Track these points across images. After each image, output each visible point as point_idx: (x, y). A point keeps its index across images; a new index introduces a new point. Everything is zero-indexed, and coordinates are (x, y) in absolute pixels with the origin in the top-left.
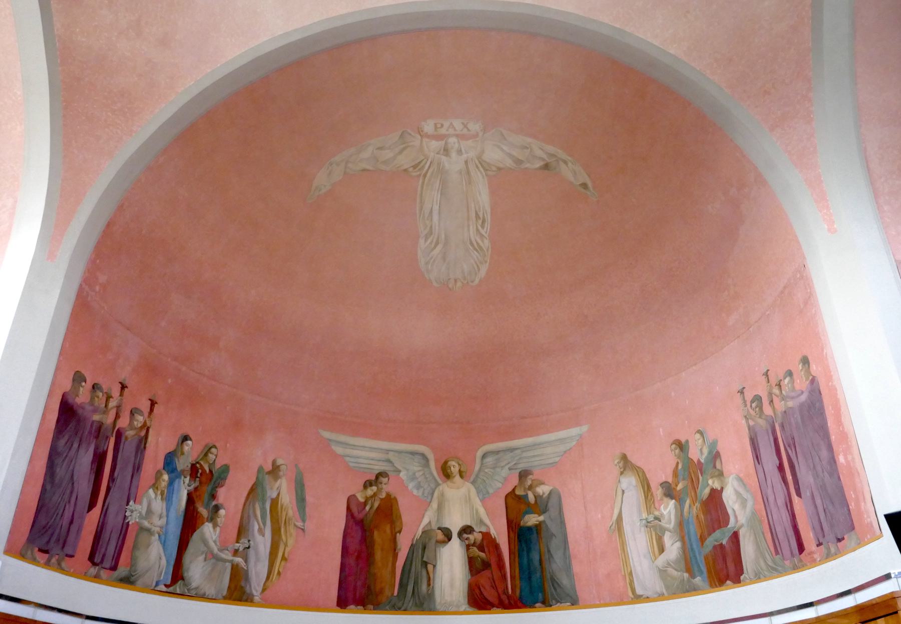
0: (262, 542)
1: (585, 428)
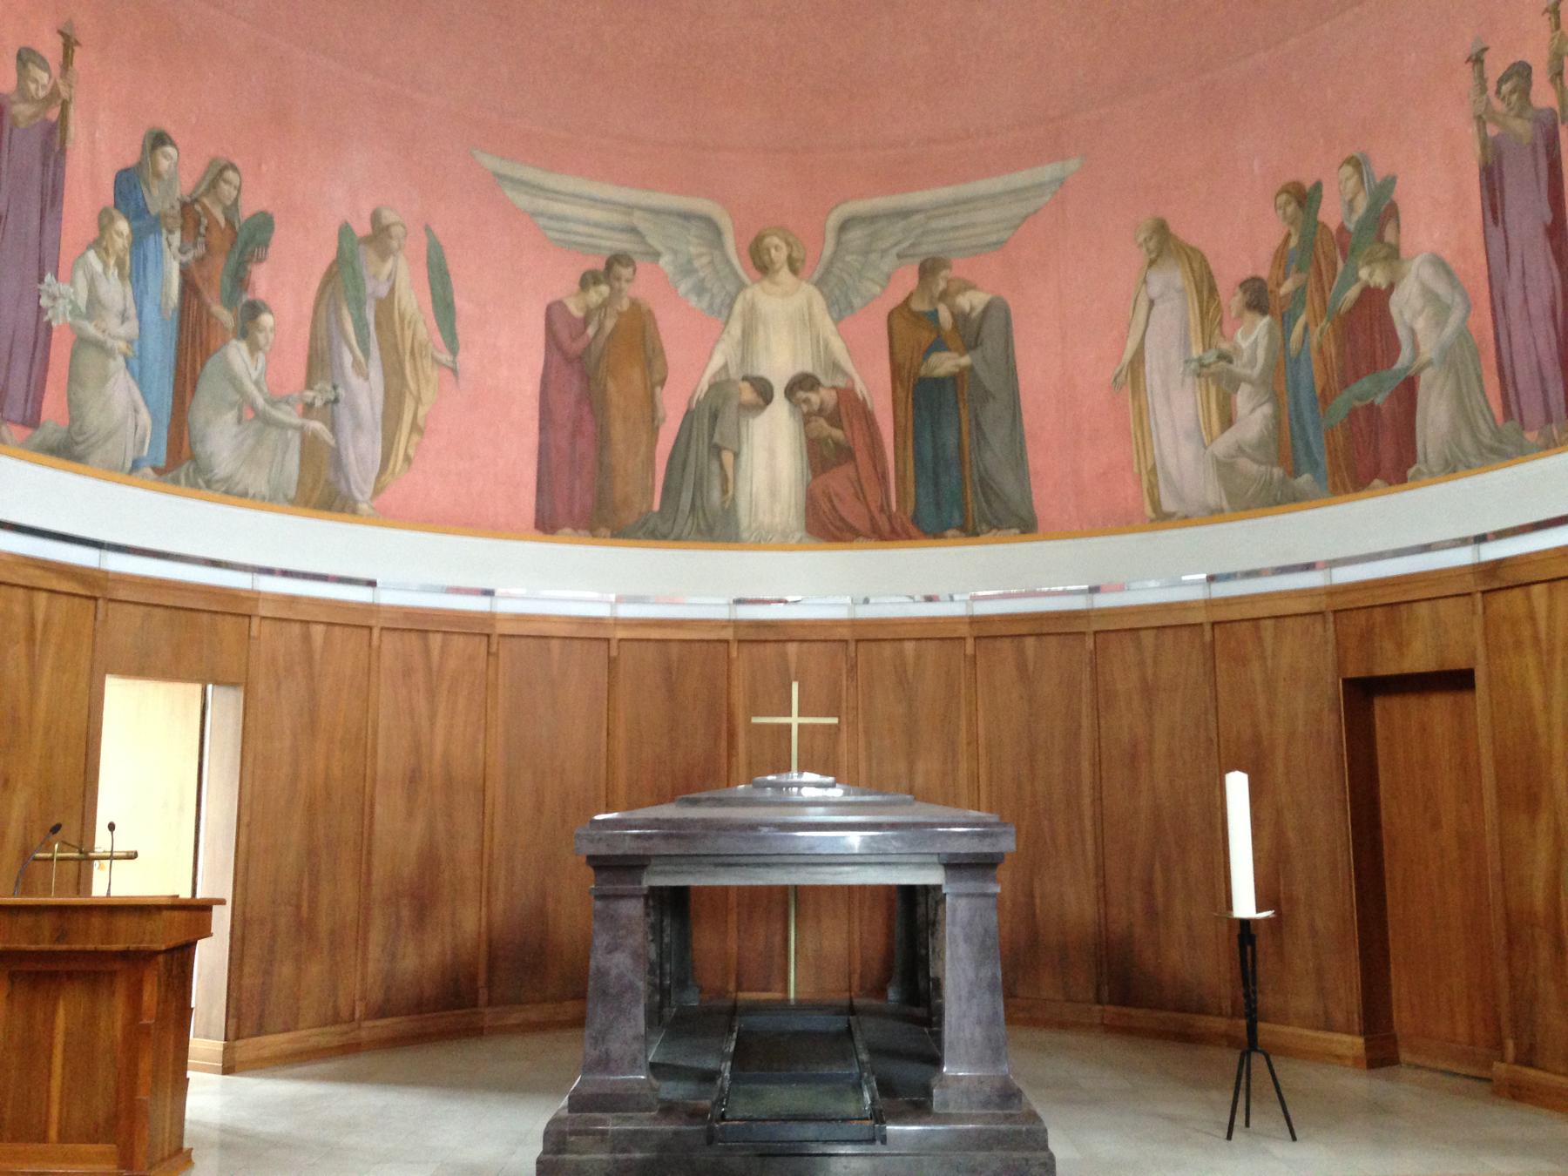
0: (365, 392)
1: (1073, 165)
